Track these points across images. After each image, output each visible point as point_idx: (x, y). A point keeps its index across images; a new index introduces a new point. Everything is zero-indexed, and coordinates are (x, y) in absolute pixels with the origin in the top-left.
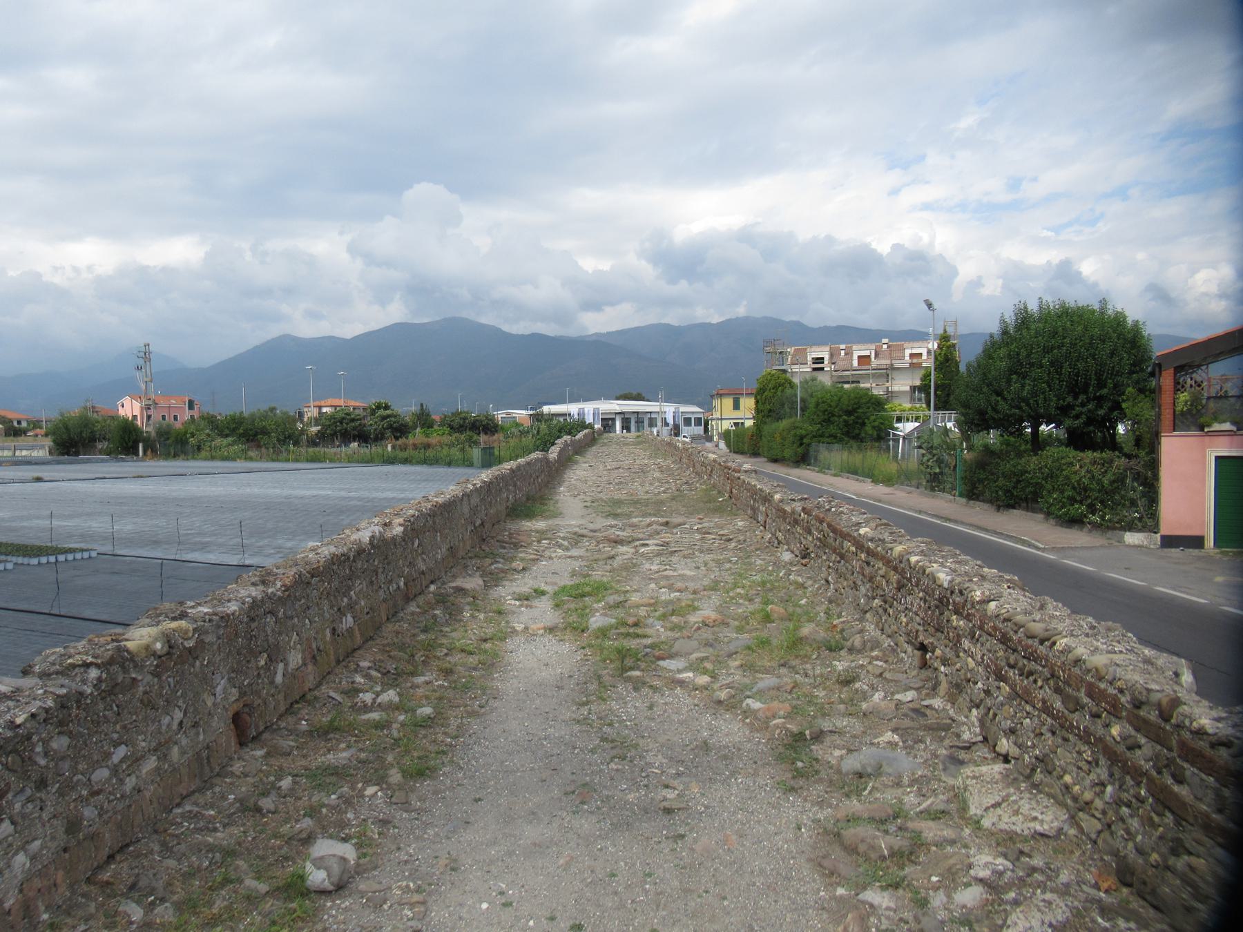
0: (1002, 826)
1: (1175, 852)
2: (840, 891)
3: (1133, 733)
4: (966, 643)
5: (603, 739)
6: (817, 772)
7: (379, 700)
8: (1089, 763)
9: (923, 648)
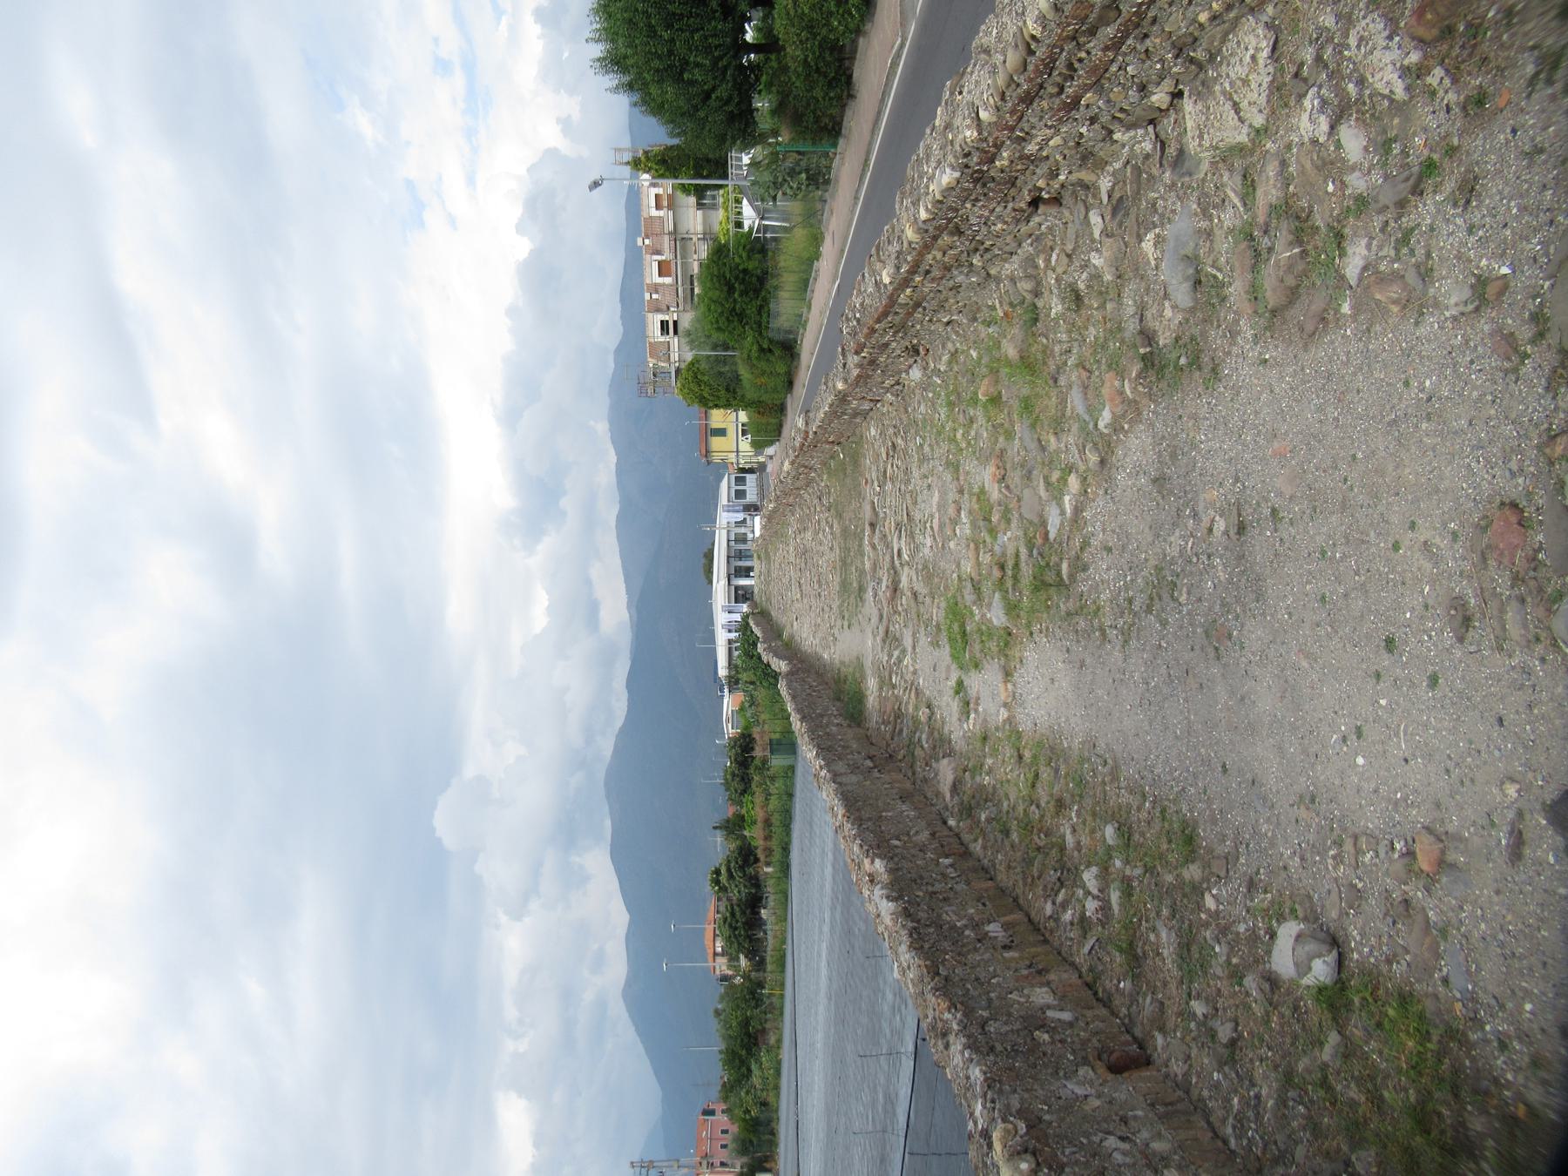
0: (1263, 100)
2: (1346, 308)
7: (1095, 892)
9: (1035, 203)
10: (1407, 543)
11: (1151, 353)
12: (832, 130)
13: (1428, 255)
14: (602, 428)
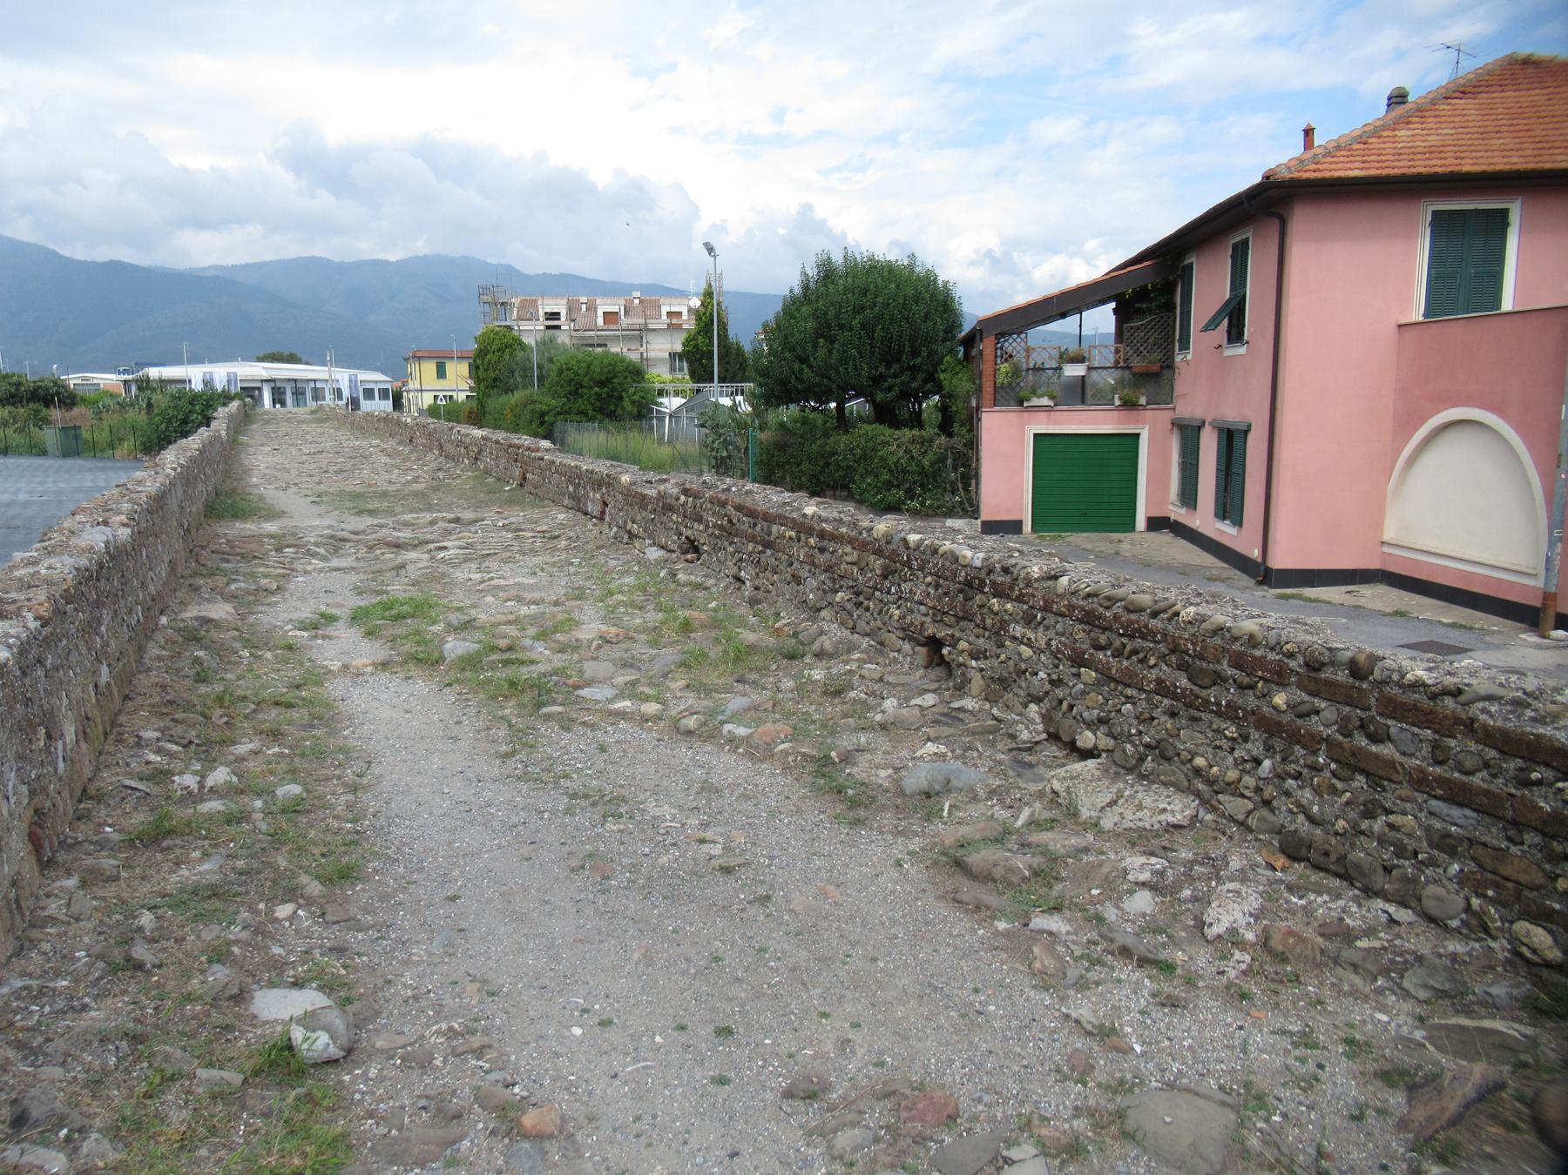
0: (1127, 824)
1: (1369, 814)
2: (1002, 925)
3: (1307, 698)
4: (1018, 630)
5: (574, 796)
6: (874, 799)
7: (210, 782)
8: (1233, 739)
9: (934, 644)
10: (837, 1025)
11: (834, 763)
12: (769, 477)
13: (1098, 984)
14: (422, 247)
